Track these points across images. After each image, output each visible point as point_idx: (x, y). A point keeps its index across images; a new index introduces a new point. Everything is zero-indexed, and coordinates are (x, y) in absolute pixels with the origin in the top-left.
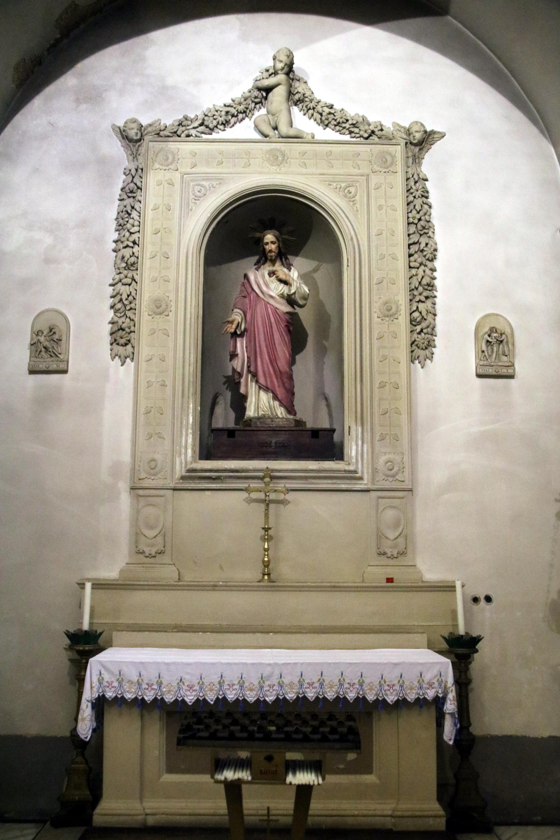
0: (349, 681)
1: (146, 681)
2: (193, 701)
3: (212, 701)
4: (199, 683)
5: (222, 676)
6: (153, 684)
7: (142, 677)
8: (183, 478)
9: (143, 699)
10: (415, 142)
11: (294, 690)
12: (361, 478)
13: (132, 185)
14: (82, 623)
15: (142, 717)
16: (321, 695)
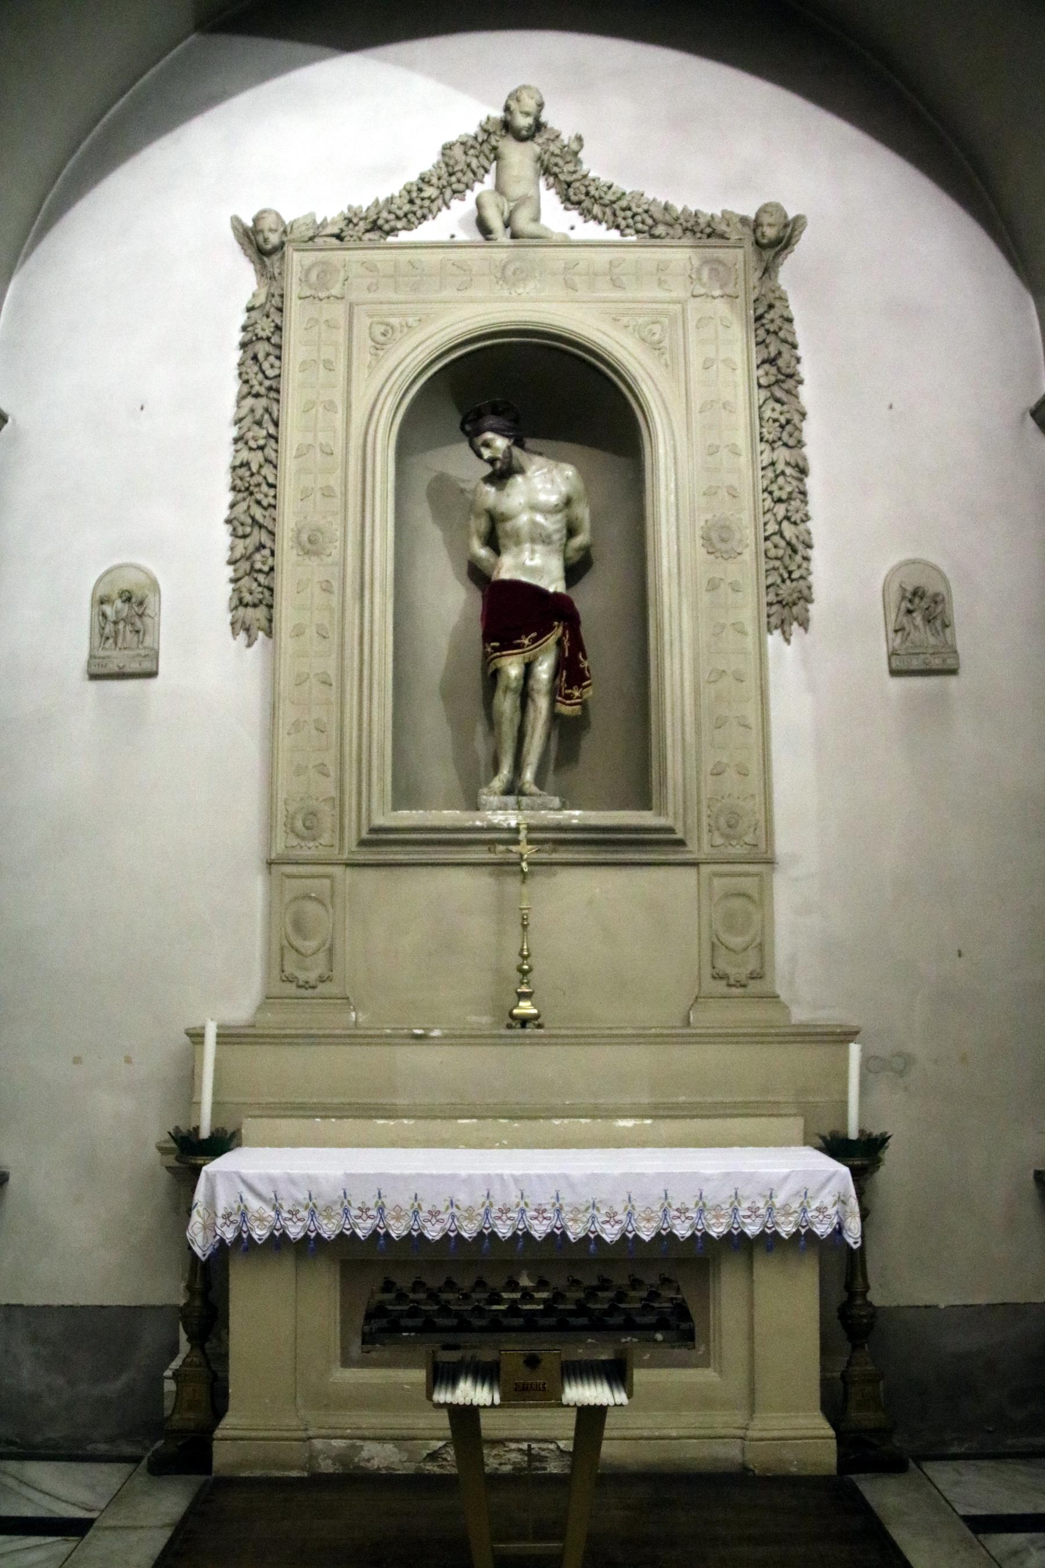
0: (360, 1205)
1: (357, 1204)
2: (264, 1238)
3: (260, 1239)
4: (483, 1204)
5: (379, 1194)
6: (368, 1209)
7: (492, 1200)
8: (362, 843)
9: (459, 1236)
10: (765, 241)
11: (722, 1220)
12: (681, 843)
13: (336, 291)
14: (200, 1103)
15: (297, 1267)
16: (381, 1228)
